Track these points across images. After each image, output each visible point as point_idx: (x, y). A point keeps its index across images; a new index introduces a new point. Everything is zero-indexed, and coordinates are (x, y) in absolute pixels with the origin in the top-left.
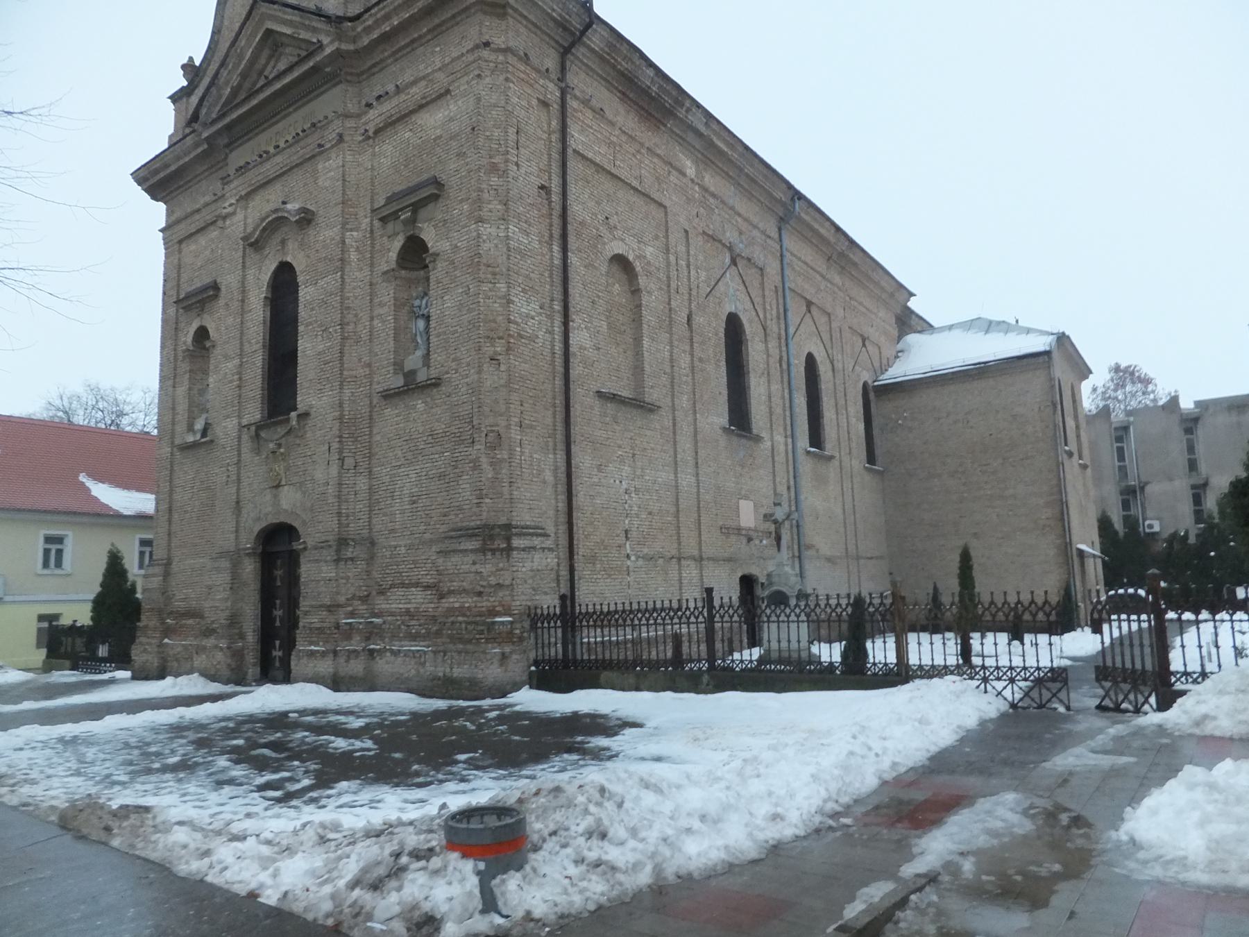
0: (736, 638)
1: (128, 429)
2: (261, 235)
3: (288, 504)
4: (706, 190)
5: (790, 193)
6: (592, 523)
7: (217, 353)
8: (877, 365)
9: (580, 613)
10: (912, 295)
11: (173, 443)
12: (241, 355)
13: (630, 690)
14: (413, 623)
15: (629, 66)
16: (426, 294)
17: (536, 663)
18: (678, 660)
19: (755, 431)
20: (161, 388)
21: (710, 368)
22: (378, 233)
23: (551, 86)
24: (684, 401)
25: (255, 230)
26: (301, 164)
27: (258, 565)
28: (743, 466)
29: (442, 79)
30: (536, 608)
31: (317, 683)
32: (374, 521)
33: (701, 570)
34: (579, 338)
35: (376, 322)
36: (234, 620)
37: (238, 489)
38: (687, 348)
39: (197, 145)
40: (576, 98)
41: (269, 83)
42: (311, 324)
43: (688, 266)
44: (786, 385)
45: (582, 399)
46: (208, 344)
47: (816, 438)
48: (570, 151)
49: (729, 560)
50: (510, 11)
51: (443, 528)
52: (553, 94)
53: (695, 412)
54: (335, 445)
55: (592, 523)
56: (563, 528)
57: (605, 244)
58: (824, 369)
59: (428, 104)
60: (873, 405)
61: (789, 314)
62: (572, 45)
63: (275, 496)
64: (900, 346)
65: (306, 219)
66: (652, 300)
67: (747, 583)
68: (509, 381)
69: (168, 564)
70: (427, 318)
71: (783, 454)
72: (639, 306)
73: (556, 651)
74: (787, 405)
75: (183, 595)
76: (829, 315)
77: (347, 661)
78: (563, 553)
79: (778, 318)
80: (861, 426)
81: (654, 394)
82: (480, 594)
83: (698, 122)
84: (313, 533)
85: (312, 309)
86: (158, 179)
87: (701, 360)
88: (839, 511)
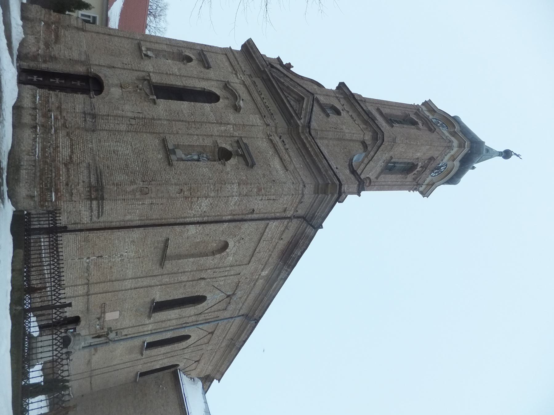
0: (43, 318)
1: (148, 19)
2: (229, 89)
3: (113, 92)
4: (257, 281)
5: (257, 318)
6: (105, 239)
7: (181, 65)
8: (187, 369)
9: (57, 237)
10: (219, 381)
11: (142, 40)
12: (180, 76)
13: (12, 266)
14: (52, 149)
15: (301, 245)
16: (208, 159)
17: (29, 214)
18: (31, 290)
19: (153, 315)
20: (166, 39)
21: (182, 290)
22: (232, 139)
23: (292, 213)
24: (166, 279)
25: (232, 87)
26: (258, 108)
27: (82, 74)
28: (136, 311)
29: (291, 168)
30: (60, 213)
31: (18, 98)
32: (105, 132)
33: (82, 296)
34: (192, 229)
35: (196, 137)
36: (53, 59)
37: (120, 68)
38: (190, 279)
39: (262, 66)
40: (288, 223)
41: (286, 97)
42: (195, 108)
43: (225, 276)
44: (176, 327)
45: (165, 232)
46: (185, 61)
47: (152, 345)
48: (268, 221)
49: (88, 309)
50: (317, 195)
51: (102, 167)
52: (289, 214)
53: (161, 285)
54: (141, 116)
55: (105, 239)
56: (103, 225)
57: (232, 238)
58: (184, 344)
59: (282, 162)
60: (169, 371)
61: (207, 325)
62: (307, 221)
63: (117, 85)
64: (196, 379)
65: (237, 109)
66: (210, 261)
67: (76, 320)
68: (172, 198)
69: (83, 30)
70: (198, 160)
71: (142, 330)
72: (207, 255)
73: (35, 225)
74: (166, 329)
75: (67, 35)
76: (208, 343)
77: (30, 114)
78: (90, 226)
79: (205, 320)
80: (158, 367)
81: (169, 265)
82: (67, 184)
83: (282, 276)
84: (99, 103)
85: (200, 109)
86: (249, 48)
87: (185, 286)
88: (115, 363)
